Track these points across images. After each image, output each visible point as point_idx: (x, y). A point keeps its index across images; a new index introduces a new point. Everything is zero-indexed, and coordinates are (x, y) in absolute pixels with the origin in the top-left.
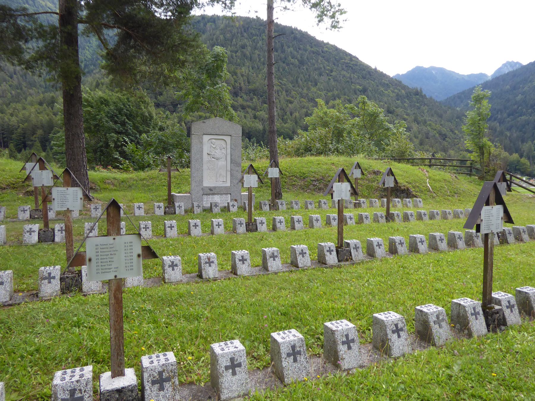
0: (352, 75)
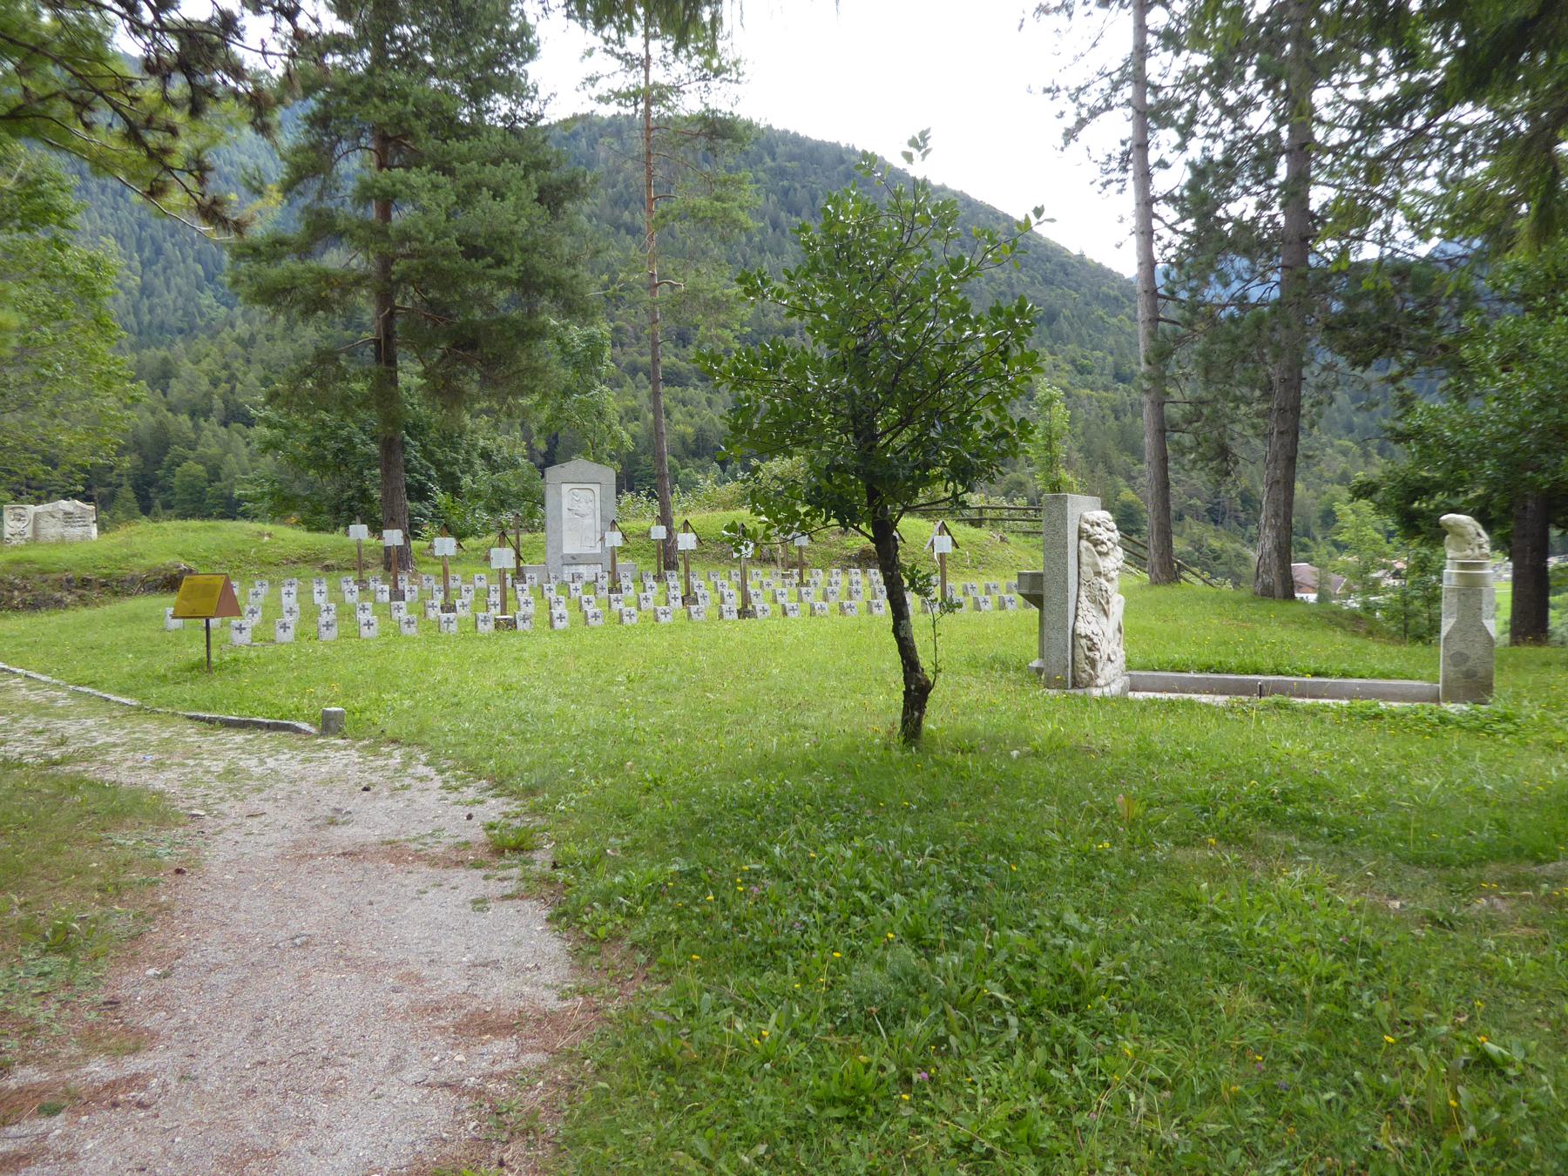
0: (1014, 275)
